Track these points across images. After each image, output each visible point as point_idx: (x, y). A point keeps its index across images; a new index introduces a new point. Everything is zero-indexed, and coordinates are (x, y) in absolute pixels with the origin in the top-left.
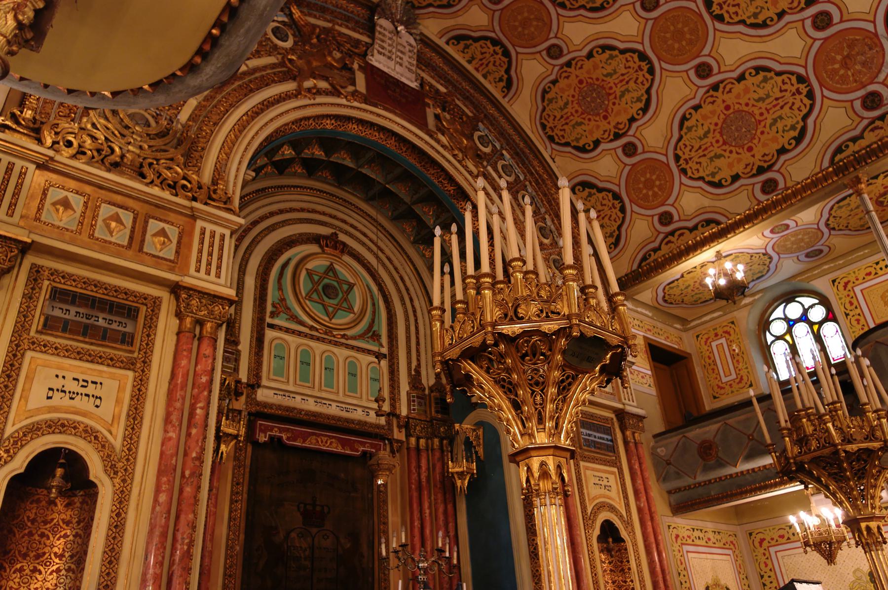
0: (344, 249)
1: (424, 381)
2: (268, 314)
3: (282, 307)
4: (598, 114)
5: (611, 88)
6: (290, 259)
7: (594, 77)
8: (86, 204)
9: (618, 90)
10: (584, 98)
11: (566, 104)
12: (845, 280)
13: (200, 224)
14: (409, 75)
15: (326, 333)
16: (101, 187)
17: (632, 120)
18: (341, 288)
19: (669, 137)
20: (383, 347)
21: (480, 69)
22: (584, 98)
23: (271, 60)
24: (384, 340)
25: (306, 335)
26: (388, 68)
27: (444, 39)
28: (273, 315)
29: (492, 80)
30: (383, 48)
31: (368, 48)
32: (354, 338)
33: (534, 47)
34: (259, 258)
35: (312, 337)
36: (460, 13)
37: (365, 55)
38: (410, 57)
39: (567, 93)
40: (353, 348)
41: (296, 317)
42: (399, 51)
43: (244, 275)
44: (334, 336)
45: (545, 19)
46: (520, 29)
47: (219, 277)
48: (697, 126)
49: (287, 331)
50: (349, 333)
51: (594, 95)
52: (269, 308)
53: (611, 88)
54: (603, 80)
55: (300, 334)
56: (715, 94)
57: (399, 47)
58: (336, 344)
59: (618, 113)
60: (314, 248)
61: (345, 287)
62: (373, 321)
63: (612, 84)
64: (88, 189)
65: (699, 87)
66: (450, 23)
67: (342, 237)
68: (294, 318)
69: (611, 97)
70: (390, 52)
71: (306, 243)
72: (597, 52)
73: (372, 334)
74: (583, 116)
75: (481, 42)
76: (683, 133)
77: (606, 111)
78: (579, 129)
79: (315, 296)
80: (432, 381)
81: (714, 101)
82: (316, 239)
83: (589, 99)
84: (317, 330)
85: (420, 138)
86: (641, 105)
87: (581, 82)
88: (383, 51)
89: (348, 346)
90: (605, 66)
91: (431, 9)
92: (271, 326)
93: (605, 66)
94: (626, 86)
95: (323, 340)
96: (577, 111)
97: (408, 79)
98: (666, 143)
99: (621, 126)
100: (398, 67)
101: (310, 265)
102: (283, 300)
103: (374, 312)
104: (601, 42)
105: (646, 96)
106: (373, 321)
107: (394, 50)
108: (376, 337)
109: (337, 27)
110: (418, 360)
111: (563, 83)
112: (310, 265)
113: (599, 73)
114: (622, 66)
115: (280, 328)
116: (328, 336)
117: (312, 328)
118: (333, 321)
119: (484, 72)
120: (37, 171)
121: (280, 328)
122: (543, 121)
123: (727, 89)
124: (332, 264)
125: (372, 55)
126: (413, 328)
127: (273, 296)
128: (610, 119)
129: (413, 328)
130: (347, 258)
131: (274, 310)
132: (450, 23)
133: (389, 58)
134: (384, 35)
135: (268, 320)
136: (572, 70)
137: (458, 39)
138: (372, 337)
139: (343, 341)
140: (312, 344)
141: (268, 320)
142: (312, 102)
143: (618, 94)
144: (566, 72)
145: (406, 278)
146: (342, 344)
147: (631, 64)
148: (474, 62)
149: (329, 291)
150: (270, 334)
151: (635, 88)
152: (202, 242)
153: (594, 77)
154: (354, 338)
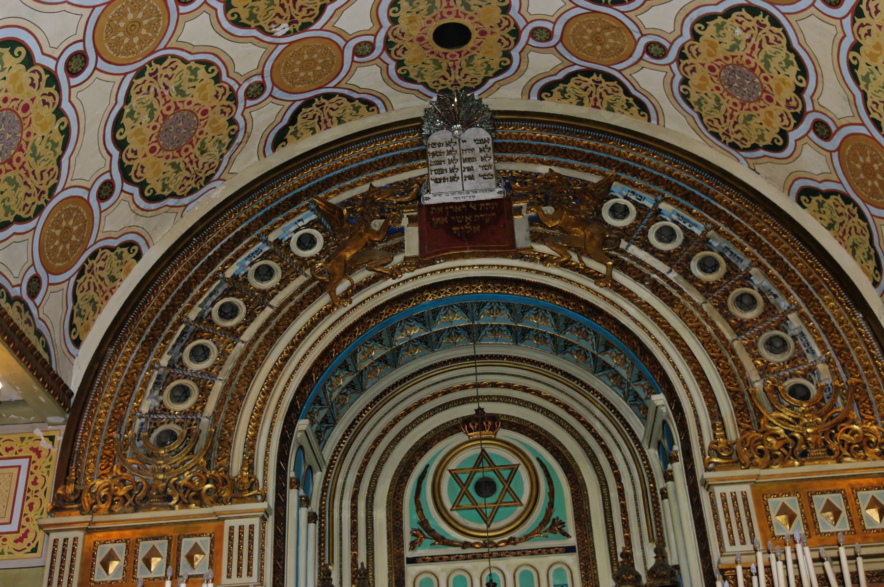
0: (496, 422)
1: (639, 568)
2: (407, 546)
3: (425, 529)
4: (759, 99)
5: (748, 62)
6: (427, 466)
7: (721, 57)
8: (127, 548)
9: (758, 60)
10: (731, 86)
11: (717, 100)
12: (19, 546)
13: (228, 524)
14: (485, 184)
15: (485, 545)
16: (137, 527)
17: (799, 91)
18: (499, 475)
19: (851, 98)
20: (568, 536)
21: (598, 104)
22: (731, 86)
23: (301, 280)
24: (571, 527)
25: (458, 558)
26: (453, 193)
27: (534, 97)
28: (413, 545)
29: (620, 109)
30: (441, 171)
31: (421, 185)
32: (527, 538)
33: (631, 56)
34: (388, 481)
35: (466, 557)
36: (522, 68)
37: (418, 197)
38: (482, 159)
39: (708, 88)
40: (524, 553)
41: (443, 538)
42: (466, 160)
43: (372, 510)
44: (496, 546)
45: (614, 24)
46: (599, 48)
47: (251, 576)
48: (872, 73)
49: (433, 559)
50: (516, 534)
51: (738, 78)
52: (408, 538)
53: (748, 62)
54: (733, 57)
55: (449, 558)
56: (863, 21)
57: (466, 155)
58: (500, 555)
59: (779, 90)
60: (459, 438)
61: (506, 474)
62: (551, 505)
63: (746, 57)
64: (128, 533)
65: (841, 19)
66: (523, 81)
67: (490, 408)
68: (443, 541)
69: (757, 71)
70: (452, 171)
71: (445, 437)
72: (700, 28)
73: (558, 527)
74: (746, 107)
75: (573, 80)
76: (862, 87)
77: (764, 91)
78: (753, 124)
79: (465, 502)
80: (651, 562)
81: (869, 31)
82: (465, 424)
83: (736, 85)
84: (472, 545)
85: (509, 267)
86: (794, 69)
87: (712, 69)
88: (442, 176)
89: (516, 553)
90: (721, 39)
91: (491, 81)
92: (413, 561)
93: (721, 39)
94: (762, 53)
95: (481, 556)
96: (735, 104)
97: (484, 191)
98: (854, 108)
99: (793, 103)
100: (468, 184)
101: (453, 465)
102: (424, 523)
103: (551, 494)
104: (695, 15)
105: (792, 57)
106: (551, 505)
107: (458, 165)
108: (558, 527)
109: (377, 183)
110: (628, 540)
111: (694, 79)
112: (453, 465)
113: (721, 51)
114: (738, 31)
115: (424, 560)
116: (489, 549)
117: (465, 545)
118: (493, 526)
119: (605, 105)
120: (87, 536)
121: (424, 560)
122: (710, 129)
123: (873, 10)
124: (483, 450)
125: (429, 191)
126: (614, 495)
127: (411, 522)
128: (775, 99)
129: (614, 495)
130: (504, 434)
131: (414, 538)
132: (523, 81)
133: (453, 179)
134: (441, 153)
135: (408, 554)
136: (690, 60)
137: (548, 89)
138: (551, 530)
139: (511, 547)
140: (467, 565)
141: (408, 554)
142: (349, 306)
143: (762, 65)
144: (686, 65)
145: (598, 426)
146: (508, 554)
147: (746, 24)
148: (586, 101)
149: (485, 487)
150: (411, 571)
151: (774, 50)
152: (231, 539)
153: (721, 57)
154: (527, 538)
